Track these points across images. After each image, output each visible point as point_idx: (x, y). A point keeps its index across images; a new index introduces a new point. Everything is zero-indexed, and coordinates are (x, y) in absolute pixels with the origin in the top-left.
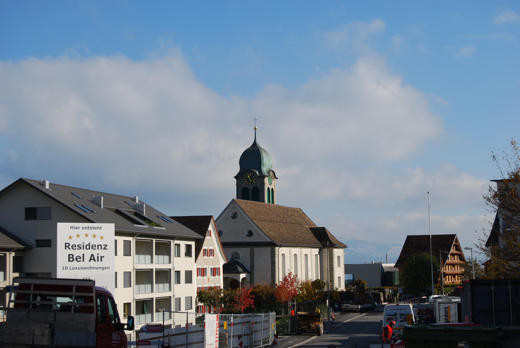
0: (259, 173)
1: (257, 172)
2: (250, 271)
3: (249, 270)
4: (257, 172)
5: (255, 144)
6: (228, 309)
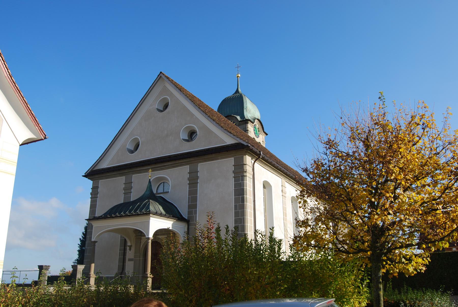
0: (241, 118)
1: (238, 118)
2: (186, 218)
3: (185, 216)
4: (238, 118)
5: (237, 91)
6: (332, 294)
